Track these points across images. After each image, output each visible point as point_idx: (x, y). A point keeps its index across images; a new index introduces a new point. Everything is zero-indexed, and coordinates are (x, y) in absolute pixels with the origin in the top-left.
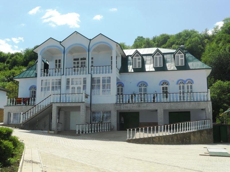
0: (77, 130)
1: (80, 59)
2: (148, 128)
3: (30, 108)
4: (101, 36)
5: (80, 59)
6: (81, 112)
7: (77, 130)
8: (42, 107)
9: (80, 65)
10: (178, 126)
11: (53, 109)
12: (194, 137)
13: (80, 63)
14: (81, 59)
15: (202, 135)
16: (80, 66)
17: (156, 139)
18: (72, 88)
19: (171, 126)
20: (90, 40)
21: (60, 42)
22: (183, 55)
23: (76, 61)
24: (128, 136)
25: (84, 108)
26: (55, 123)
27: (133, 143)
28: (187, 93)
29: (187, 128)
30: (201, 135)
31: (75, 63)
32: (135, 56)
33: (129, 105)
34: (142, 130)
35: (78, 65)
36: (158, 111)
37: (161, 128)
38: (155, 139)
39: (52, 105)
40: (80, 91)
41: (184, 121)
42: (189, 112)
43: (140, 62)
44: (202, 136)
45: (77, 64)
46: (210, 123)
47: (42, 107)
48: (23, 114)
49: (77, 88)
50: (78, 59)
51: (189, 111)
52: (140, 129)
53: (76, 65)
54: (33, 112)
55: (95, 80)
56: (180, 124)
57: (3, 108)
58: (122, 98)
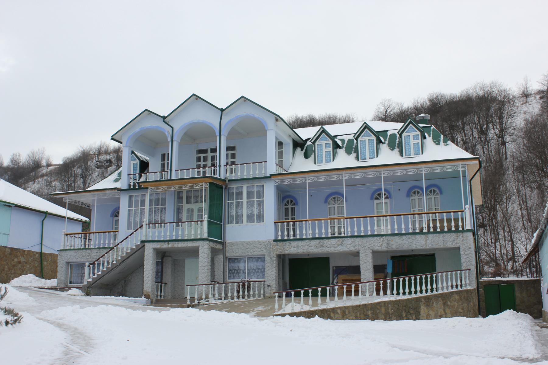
0: (188, 297)
1: (209, 151)
2: (320, 290)
3: (103, 254)
4: (245, 101)
5: (209, 151)
6: (200, 259)
7: (188, 297)
8: (125, 250)
10: (413, 281)
11: (146, 254)
12: (427, 309)
13: (209, 159)
15: (449, 303)
16: (209, 165)
17: (337, 313)
18: (188, 210)
19: (400, 281)
20: (222, 110)
21: (164, 118)
22: (419, 133)
23: (202, 156)
24: (276, 306)
25: (206, 250)
26: (150, 282)
27: (388, 317)
28: (161, 223)
29: (424, 288)
30: (445, 304)
31: (199, 159)
32: (320, 141)
33: (441, 237)
34: (297, 295)
35: (205, 163)
36: (361, 255)
37: (341, 289)
38: (334, 313)
39: (144, 246)
40: (192, 216)
41: (420, 272)
42: (433, 256)
43: (330, 151)
44: (448, 305)
45: (204, 161)
46: (469, 279)
47: (125, 250)
48: (89, 266)
49: (194, 211)
50: (205, 151)
51: (432, 253)
52: (302, 292)
53: (202, 163)
54: (108, 262)
55: (233, 193)
56: (413, 278)
57: (57, 253)
58: (462, 219)
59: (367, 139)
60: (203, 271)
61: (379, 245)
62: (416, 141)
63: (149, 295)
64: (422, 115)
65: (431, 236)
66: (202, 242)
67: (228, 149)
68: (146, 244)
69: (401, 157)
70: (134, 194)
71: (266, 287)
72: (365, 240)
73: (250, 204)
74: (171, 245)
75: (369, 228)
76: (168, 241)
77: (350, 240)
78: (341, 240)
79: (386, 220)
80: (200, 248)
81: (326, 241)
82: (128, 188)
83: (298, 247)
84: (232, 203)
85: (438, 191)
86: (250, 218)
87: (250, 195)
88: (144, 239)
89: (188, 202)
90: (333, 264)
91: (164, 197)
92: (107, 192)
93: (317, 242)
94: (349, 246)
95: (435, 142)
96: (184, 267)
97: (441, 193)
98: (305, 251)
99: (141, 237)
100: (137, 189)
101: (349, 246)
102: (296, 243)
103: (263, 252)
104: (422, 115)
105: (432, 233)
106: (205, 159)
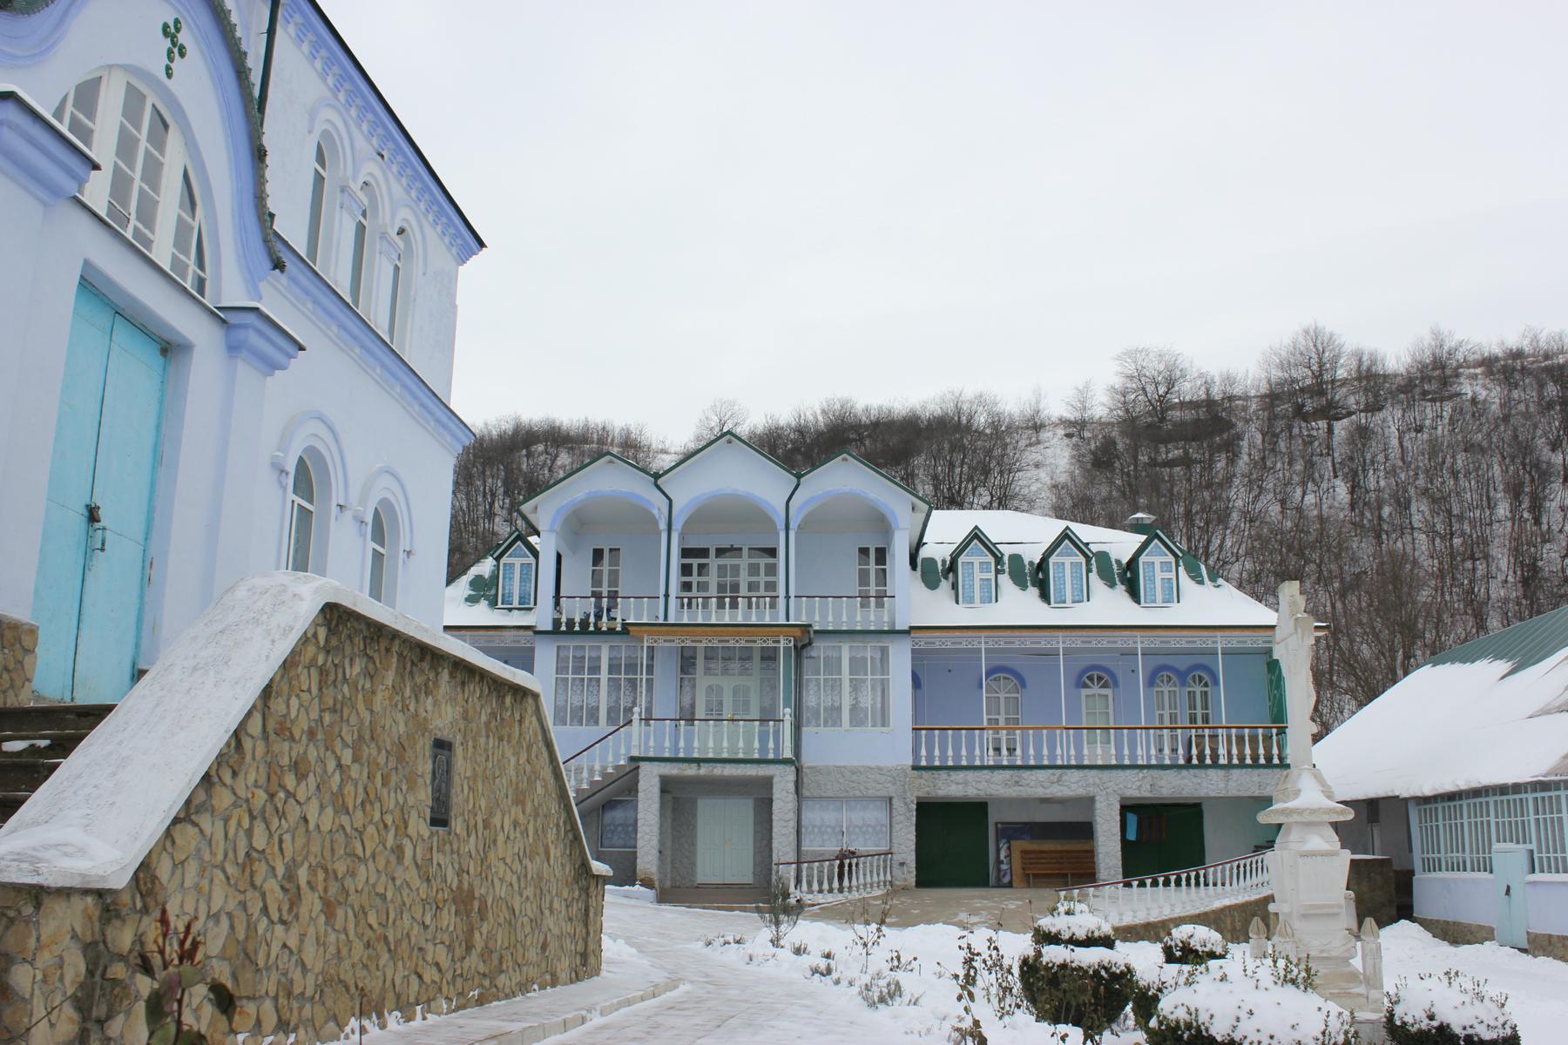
1: (712, 553)
5: (712, 553)
9: (713, 579)
14: (720, 552)
23: (695, 562)
40: (746, 704)
50: (704, 553)
59: (1067, 561)
60: (784, 831)
61: (1139, 787)
62: (985, 576)
63: (651, 880)
64: (1139, 515)
65: (1236, 773)
66: (781, 767)
67: (686, 553)
68: (642, 764)
69: (1045, 605)
70: (571, 643)
71: (895, 865)
72: (1106, 774)
73: (614, 685)
74: (704, 770)
75: (950, 753)
76: (698, 761)
77: (1075, 775)
78: (1058, 772)
79: (1148, 737)
80: (775, 780)
81: (1026, 774)
82: (549, 627)
83: (966, 783)
84: (864, 681)
85: (1207, 678)
86: (857, 717)
87: (857, 665)
88: (635, 753)
89: (708, 671)
90: (994, 817)
91: (594, 654)
92: (507, 633)
93: (1008, 773)
94: (1072, 785)
95: (1193, 578)
96: (694, 816)
97: (1116, 684)
98: (982, 793)
99: (628, 748)
100: (577, 633)
101: (1074, 786)
102: (961, 775)
103: (891, 790)
104: (1139, 515)
105: (1236, 766)
106: (702, 568)
